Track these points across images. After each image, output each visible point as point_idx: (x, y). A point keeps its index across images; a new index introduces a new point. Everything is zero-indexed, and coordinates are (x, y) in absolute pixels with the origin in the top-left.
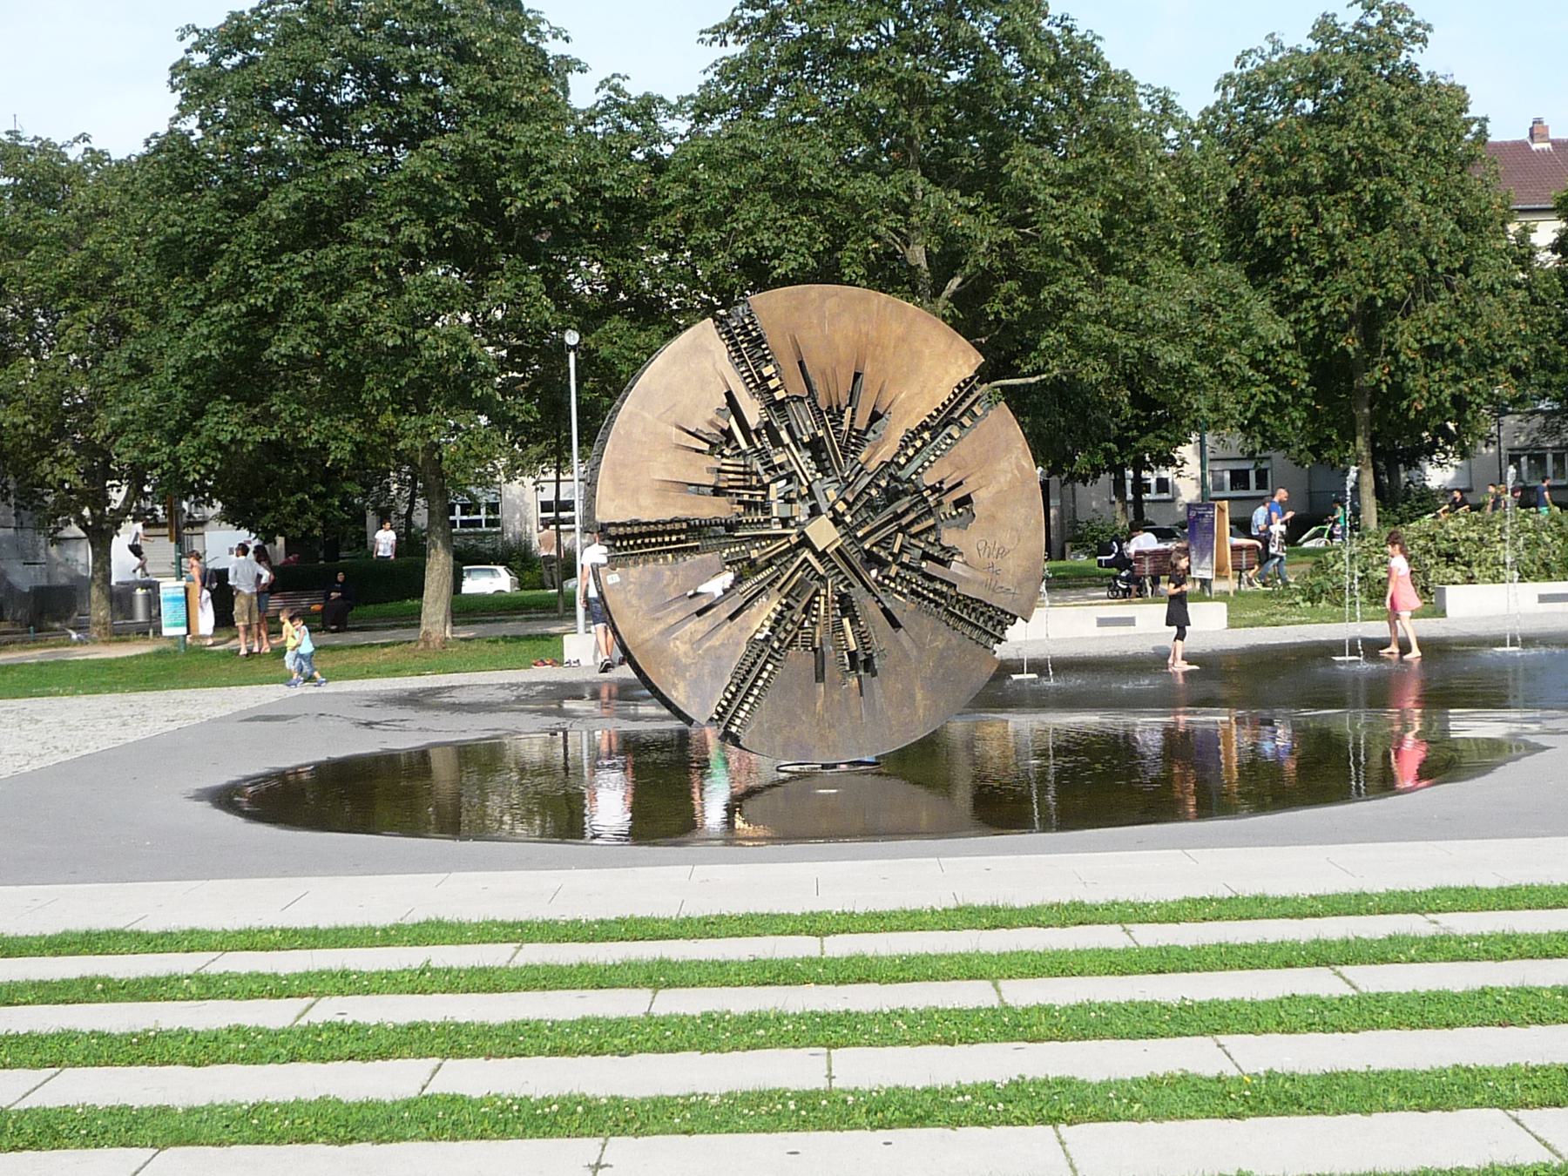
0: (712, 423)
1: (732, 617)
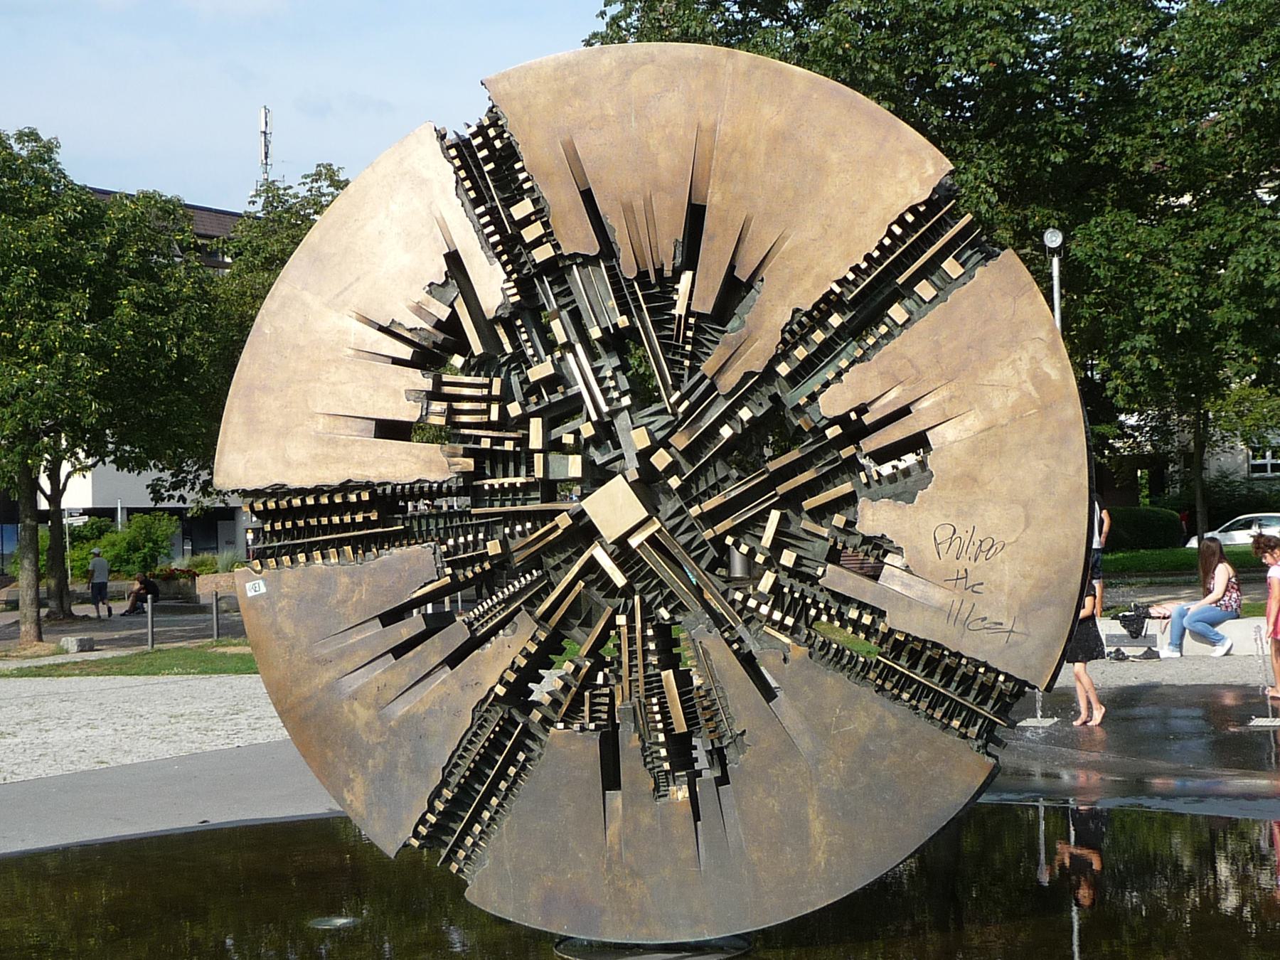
0: (419, 310)
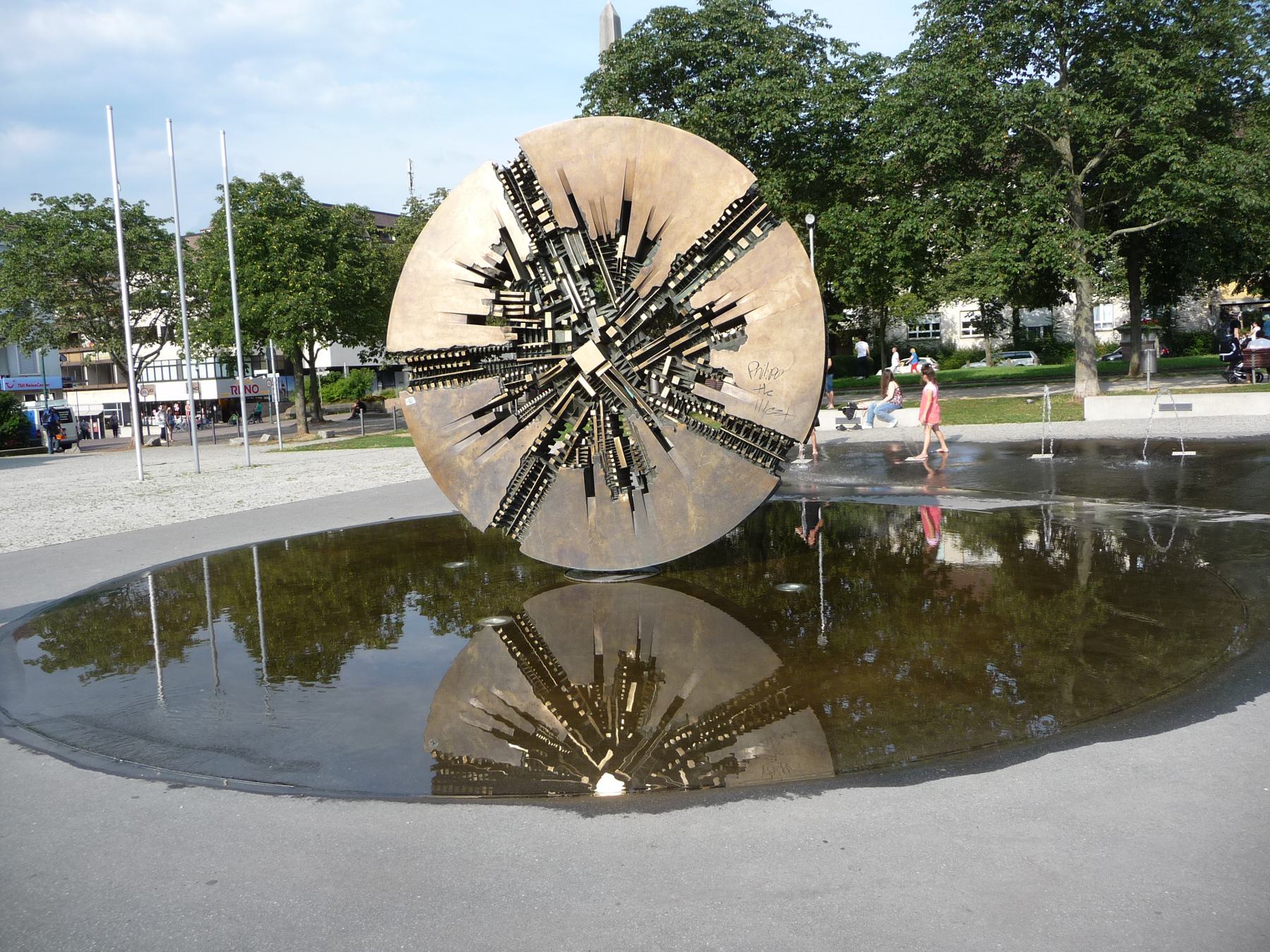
0: (487, 258)
1: (510, 434)
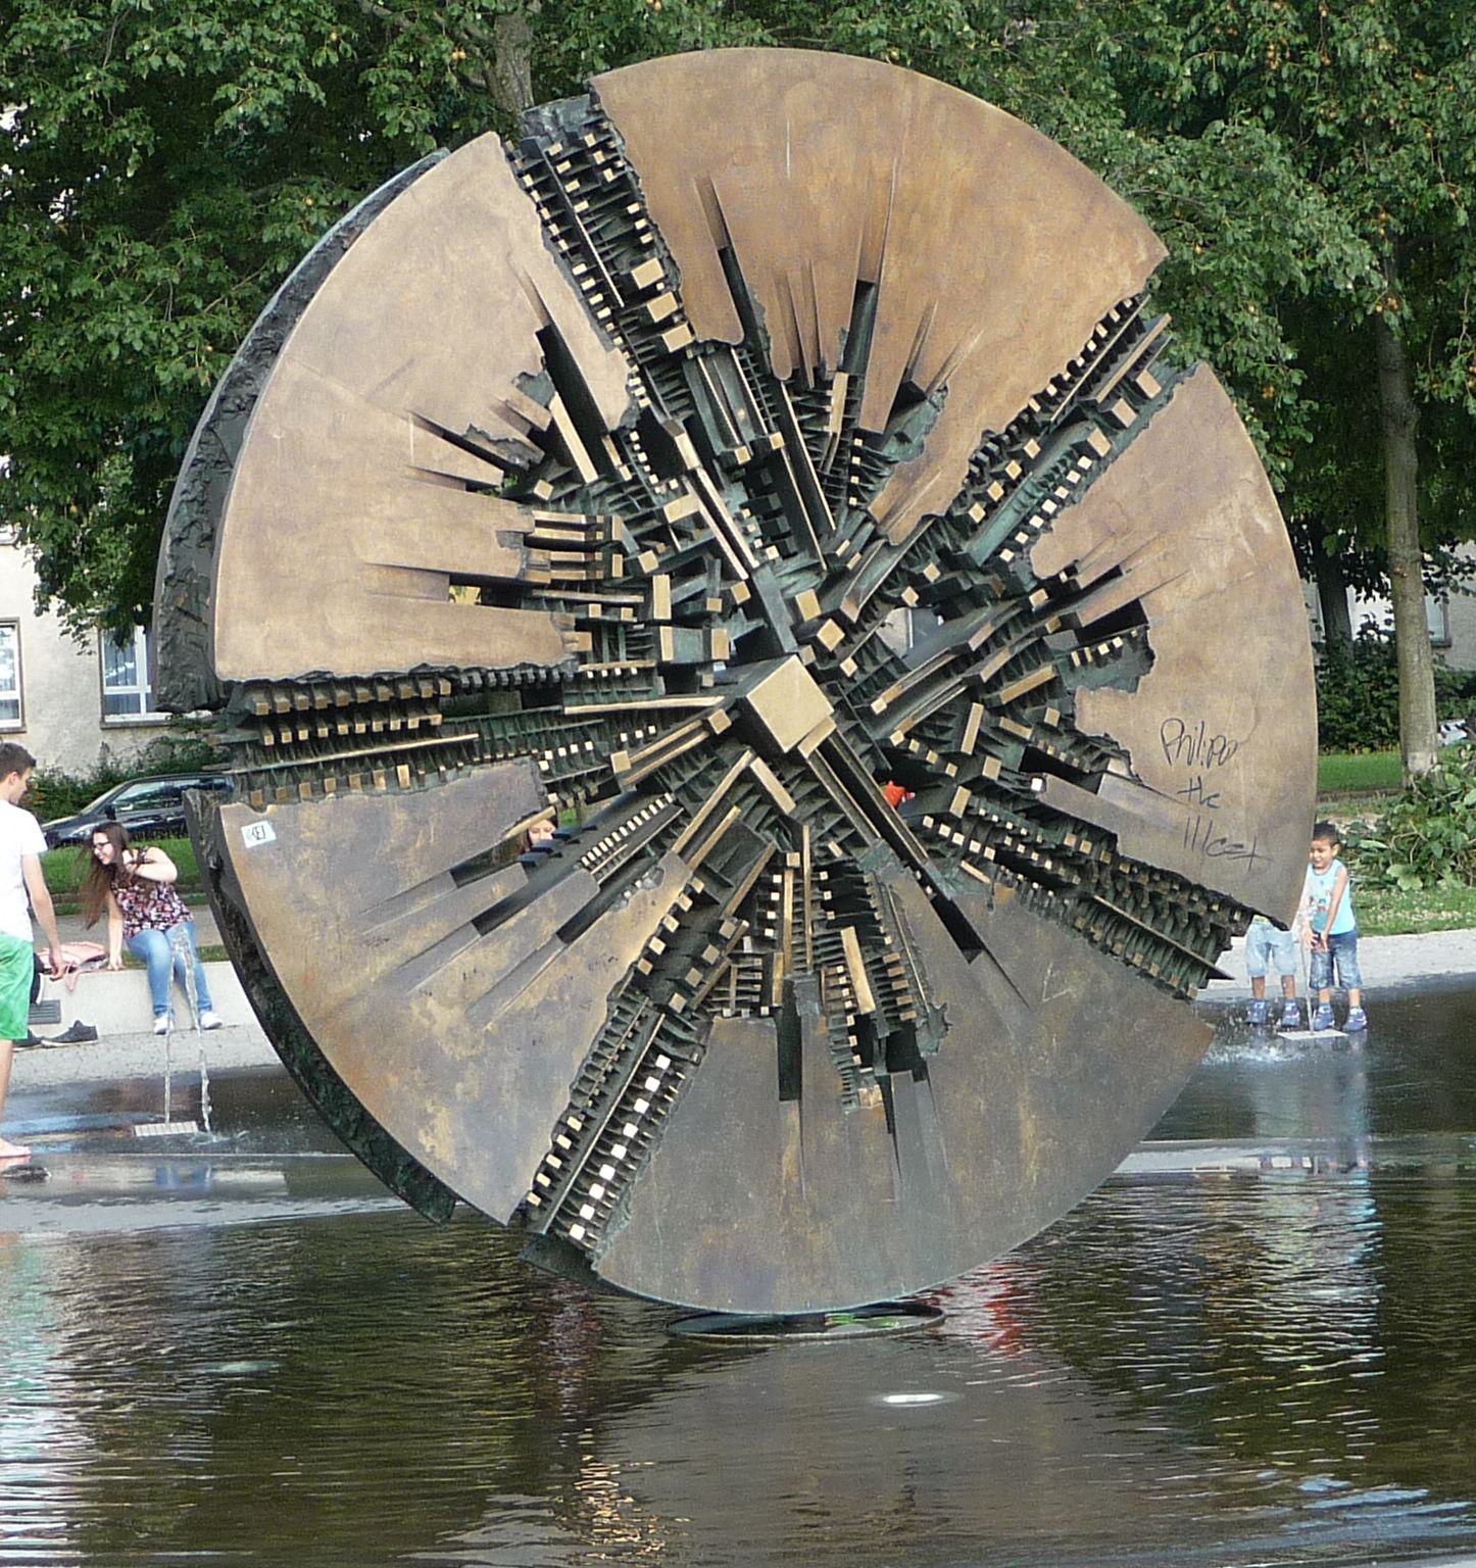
0: (508, 412)
